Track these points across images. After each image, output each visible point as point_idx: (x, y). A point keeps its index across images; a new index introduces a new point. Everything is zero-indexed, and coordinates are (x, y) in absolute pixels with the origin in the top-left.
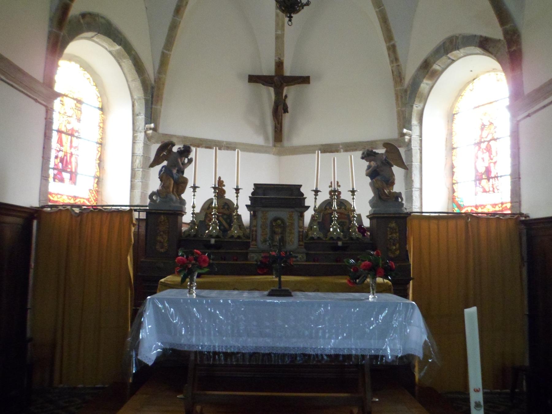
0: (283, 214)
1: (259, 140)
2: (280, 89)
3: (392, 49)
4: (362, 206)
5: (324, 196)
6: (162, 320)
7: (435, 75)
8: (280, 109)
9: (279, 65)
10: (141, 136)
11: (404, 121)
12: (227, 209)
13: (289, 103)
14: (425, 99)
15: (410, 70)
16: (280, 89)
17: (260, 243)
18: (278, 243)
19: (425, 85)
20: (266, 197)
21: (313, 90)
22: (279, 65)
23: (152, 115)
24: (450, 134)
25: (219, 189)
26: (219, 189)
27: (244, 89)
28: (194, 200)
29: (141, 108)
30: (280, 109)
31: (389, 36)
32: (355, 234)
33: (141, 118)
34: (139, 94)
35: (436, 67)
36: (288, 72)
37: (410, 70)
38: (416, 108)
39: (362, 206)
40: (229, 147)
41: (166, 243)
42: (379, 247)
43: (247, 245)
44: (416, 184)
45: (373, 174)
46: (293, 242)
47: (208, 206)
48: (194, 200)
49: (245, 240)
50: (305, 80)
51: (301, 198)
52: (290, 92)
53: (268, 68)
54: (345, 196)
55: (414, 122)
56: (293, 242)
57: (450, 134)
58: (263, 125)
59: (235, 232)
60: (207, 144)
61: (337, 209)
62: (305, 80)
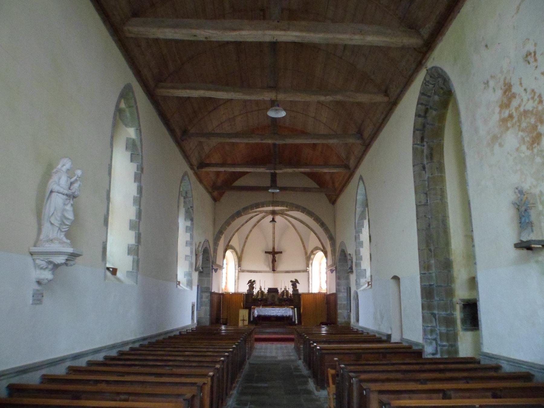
0: (274, 294)
1: (268, 269)
2: (274, 255)
3: (304, 246)
4: (291, 291)
5: (283, 289)
6: (257, 312)
7: (314, 254)
8: (274, 261)
9: (274, 248)
10: (237, 271)
11: (308, 266)
12: (262, 292)
13: (276, 259)
14: (313, 260)
15: (309, 252)
16: (274, 255)
17: (270, 299)
18: (273, 297)
19: (312, 256)
20: (270, 290)
21: (283, 255)
22: (274, 248)
23: (239, 265)
24: (320, 269)
25: (261, 289)
26: (261, 289)
27: (264, 255)
28: (255, 291)
29: (237, 263)
30: (274, 261)
31: (303, 243)
32: (289, 298)
33: (237, 266)
34: (237, 260)
35: (314, 252)
36: (276, 256)
37: (309, 252)
38: (310, 262)
39: (291, 291)
40: (260, 272)
41: (251, 300)
42: (294, 299)
43: (267, 300)
44: (310, 282)
45: (293, 285)
46: (276, 300)
47: (258, 292)
48: (255, 291)
49: (266, 300)
50: (281, 252)
51: (278, 291)
52: (276, 256)
53: (270, 250)
54: (287, 289)
55: (310, 266)
56: (276, 300)
57: (320, 269)
58: (269, 264)
59: (264, 297)
60: (229, 242)
61: (286, 292)
62: (281, 252)
